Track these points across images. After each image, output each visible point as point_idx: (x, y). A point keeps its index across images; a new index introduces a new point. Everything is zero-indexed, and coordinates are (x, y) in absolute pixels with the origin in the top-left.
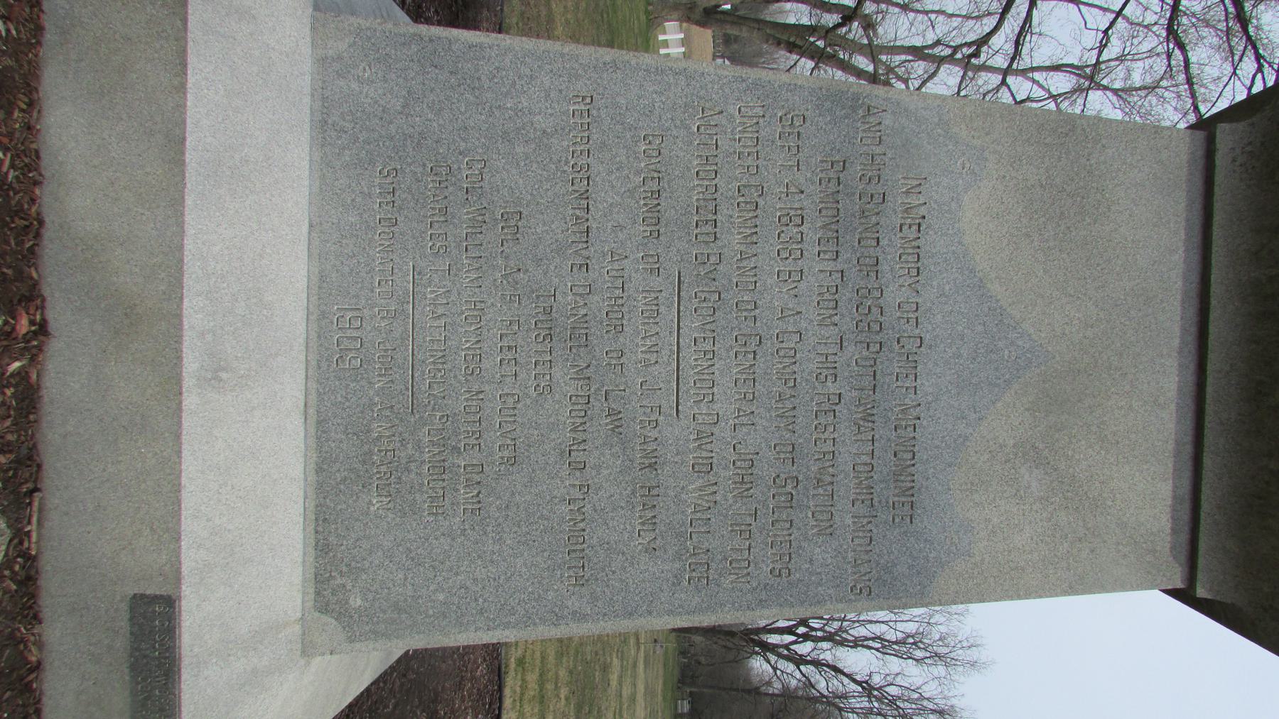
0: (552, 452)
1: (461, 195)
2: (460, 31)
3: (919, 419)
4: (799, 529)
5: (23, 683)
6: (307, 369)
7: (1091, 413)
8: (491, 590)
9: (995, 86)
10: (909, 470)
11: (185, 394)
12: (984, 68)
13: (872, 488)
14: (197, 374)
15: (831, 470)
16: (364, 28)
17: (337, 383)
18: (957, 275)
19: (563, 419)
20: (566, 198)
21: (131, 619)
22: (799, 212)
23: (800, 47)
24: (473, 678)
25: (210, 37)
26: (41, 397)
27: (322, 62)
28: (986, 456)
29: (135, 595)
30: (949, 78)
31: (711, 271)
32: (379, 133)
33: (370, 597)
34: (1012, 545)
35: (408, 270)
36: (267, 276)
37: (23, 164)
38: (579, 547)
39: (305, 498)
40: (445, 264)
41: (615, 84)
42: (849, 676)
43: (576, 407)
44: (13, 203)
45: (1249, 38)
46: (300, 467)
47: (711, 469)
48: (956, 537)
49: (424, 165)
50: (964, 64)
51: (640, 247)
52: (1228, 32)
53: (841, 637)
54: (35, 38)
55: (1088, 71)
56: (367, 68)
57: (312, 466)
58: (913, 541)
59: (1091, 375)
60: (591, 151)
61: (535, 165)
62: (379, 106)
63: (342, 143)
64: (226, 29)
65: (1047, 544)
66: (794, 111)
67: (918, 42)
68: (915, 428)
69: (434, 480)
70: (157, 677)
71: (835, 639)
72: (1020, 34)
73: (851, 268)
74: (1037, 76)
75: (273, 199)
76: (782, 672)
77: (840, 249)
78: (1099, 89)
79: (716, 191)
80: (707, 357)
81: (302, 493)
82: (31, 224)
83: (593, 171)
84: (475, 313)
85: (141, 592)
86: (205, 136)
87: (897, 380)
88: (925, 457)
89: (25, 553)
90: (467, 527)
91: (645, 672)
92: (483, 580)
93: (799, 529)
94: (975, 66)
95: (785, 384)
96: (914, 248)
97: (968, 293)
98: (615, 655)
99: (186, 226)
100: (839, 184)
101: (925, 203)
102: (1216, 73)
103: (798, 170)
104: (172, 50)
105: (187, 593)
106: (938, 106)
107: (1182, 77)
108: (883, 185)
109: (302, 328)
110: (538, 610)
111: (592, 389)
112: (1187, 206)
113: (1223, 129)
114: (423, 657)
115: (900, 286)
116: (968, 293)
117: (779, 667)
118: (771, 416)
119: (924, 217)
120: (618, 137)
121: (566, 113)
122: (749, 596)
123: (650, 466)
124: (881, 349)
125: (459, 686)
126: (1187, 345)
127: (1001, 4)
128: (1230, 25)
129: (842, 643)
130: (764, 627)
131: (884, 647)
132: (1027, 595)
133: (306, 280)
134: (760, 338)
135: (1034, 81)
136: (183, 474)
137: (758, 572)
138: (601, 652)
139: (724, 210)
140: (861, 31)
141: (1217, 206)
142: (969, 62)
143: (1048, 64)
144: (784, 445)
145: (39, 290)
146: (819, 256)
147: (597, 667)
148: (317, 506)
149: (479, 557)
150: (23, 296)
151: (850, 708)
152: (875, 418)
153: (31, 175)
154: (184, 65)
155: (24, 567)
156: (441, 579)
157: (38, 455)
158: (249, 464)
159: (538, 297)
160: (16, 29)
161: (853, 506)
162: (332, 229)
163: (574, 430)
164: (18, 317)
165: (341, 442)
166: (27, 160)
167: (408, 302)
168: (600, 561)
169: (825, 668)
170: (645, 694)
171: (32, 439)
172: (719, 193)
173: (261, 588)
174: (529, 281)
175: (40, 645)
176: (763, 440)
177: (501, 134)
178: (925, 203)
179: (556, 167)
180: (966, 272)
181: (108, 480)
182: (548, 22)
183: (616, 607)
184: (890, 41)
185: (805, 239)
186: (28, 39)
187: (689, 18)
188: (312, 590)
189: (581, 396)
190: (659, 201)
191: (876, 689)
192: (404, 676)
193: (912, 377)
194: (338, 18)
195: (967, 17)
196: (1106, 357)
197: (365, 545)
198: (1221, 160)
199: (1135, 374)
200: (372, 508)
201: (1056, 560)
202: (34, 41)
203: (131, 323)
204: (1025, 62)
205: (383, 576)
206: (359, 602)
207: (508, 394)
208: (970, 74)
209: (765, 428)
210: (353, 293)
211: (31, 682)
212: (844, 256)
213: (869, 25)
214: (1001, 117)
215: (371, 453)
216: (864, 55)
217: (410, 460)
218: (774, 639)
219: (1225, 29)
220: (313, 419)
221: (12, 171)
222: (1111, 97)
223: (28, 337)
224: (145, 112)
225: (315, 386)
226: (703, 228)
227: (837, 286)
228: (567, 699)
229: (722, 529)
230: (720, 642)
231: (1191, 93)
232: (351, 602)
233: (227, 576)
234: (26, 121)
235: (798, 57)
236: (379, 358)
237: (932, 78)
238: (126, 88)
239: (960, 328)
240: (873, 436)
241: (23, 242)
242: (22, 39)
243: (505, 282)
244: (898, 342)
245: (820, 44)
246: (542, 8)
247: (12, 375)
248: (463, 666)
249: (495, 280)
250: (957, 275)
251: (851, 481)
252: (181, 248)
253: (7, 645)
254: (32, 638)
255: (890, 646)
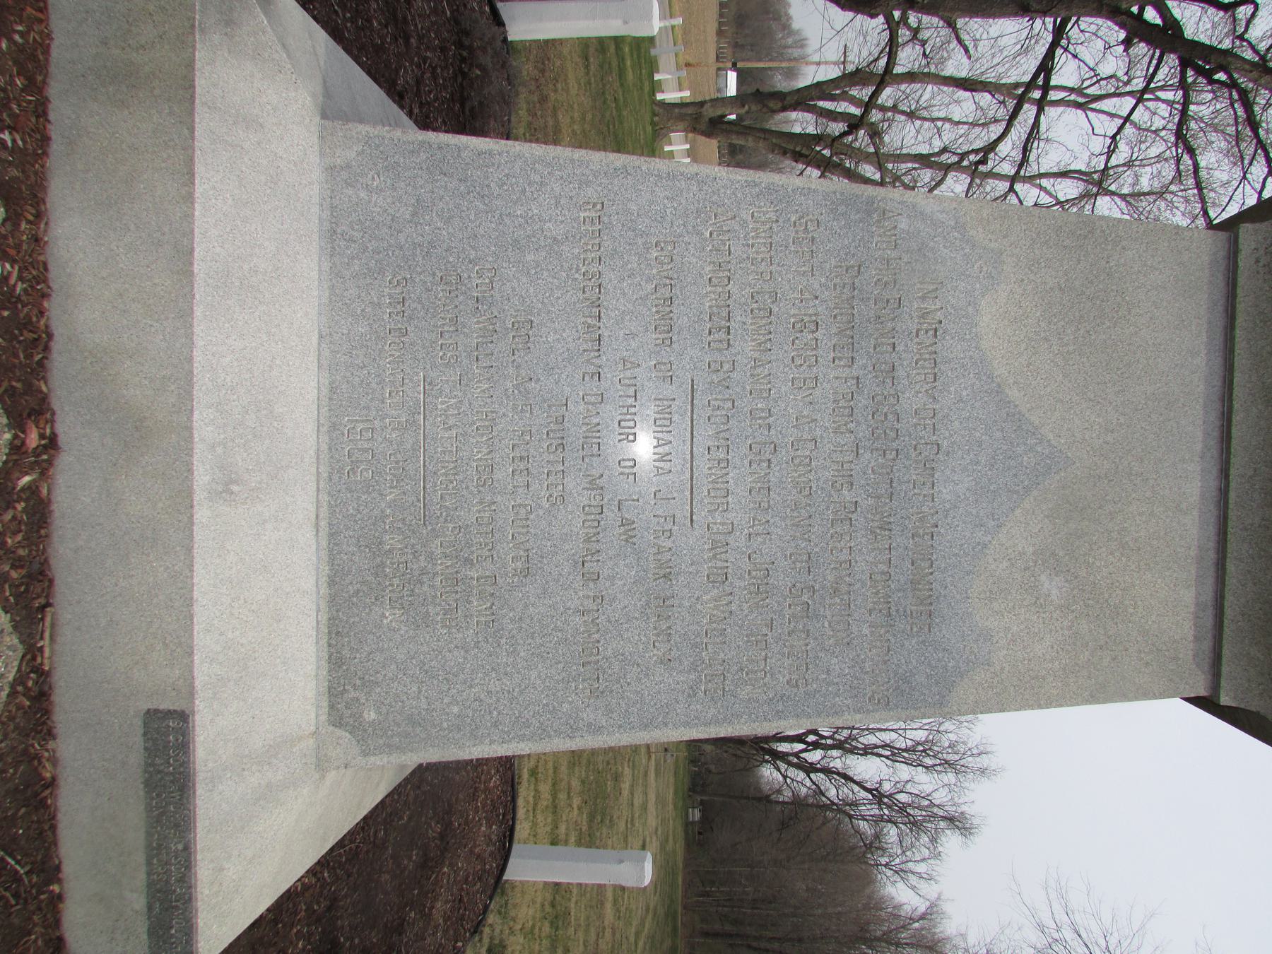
0: (566, 563)
1: (472, 303)
2: (469, 138)
3: (937, 526)
4: (816, 639)
5: (38, 798)
6: (318, 481)
7: (1112, 519)
9: (1002, 193)
10: (927, 579)
11: (196, 508)
12: (991, 175)
13: (890, 597)
14: (208, 487)
15: (847, 579)
16: (372, 135)
17: (348, 495)
18: (974, 380)
20: (577, 306)
21: (145, 734)
22: (814, 318)
23: (807, 156)
24: (487, 789)
25: (218, 146)
26: (52, 511)
27: (331, 170)
28: (1005, 564)
29: (149, 710)
30: (956, 184)
31: (724, 379)
33: (384, 710)
34: (1032, 654)
35: (419, 381)
36: (277, 387)
37: (30, 277)
38: (593, 658)
39: (318, 612)
40: (456, 373)
41: (626, 190)
42: (858, 784)
43: (589, 517)
44: (22, 315)
45: (1259, 141)
46: (312, 580)
47: (726, 578)
48: (975, 646)
49: (434, 274)
50: (970, 172)
51: (653, 355)
52: (1238, 138)
53: (851, 745)
54: (41, 149)
55: (1096, 176)
56: (376, 176)
57: (325, 579)
58: (932, 651)
59: (1112, 481)
60: (603, 259)
61: (546, 274)
62: (388, 215)
63: (351, 252)
64: (234, 138)
66: (808, 215)
67: (924, 150)
68: (932, 536)
69: (447, 592)
70: (172, 792)
71: (846, 746)
72: (1028, 140)
73: (867, 375)
74: (1045, 182)
75: (282, 310)
76: (792, 780)
77: (855, 355)
78: (1106, 195)
79: (729, 297)
80: (722, 465)
81: (314, 607)
82: (40, 337)
83: (605, 280)
84: (487, 423)
85: (155, 707)
86: (213, 247)
87: (914, 487)
88: (943, 565)
89: (38, 669)
90: (480, 639)
91: (656, 781)
92: (498, 692)
93: (816, 639)
94: (982, 173)
95: (801, 493)
96: (930, 353)
97: (986, 399)
98: (626, 765)
99: (195, 337)
100: (854, 289)
101: (942, 308)
102: (1225, 177)
103: (813, 275)
104: (179, 159)
105: (201, 708)
106: (955, 208)
107: (1191, 182)
108: (899, 290)
109: (312, 440)
110: (552, 723)
111: (605, 500)
112: (1208, 308)
113: (1246, 229)
114: (437, 769)
115: (917, 392)
116: (986, 399)
117: (789, 775)
118: (786, 525)
119: (941, 322)
121: (576, 219)
122: (766, 708)
123: (665, 576)
124: (897, 456)
125: (474, 797)
126: (1209, 450)
127: (1008, 111)
128: (1240, 129)
129: (853, 751)
130: (774, 736)
131: (894, 754)
132: (1049, 704)
133: (316, 391)
134: (775, 447)
135: (1041, 188)
136: (195, 588)
137: (775, 683)
138: (613, 762)
139: (738, 317)
140: (867, 138)
141: (1240, 307)
142: (976, 168)
143: (1055, 170)
144: (800, 555)
145: (49, 404)
146: (834, 362)
147: (609, 776)
148: (330, 619)
149: (493, 669)
150: (34, 410)
151: (861, 815)
152: (893, 526)
153: (39, 287)
154: (191, 174)
155: (37, 683)
156: (454, 691)
157: (50, 570)
158: (261, 578)
159: (549, 407)
160: (23, 140)
161: (870, 615)
162: (342, 339)
163: (588, 540)
164: (28, 431)
165: (353, 554)
166: (34, 273)
167: (419, 413)
169: (835, 776)
170: (656, 804)
171: (43, 554)
173: (275, 702)
175: (54, 761)
176: (778, 549)
178: (942, 308)
179: (568, 275)
181: (120, 595)
182: (555, 134)
183: (632, 719)
184: (897, 149)
185: (819, 345)
186: (35, 150)
187: (695, 129)
188: (325, 704)
189: (594, 506)
190: (671, 308)
191: (886, 797)
192: (419, 788)
193: (929, 485)
194: (346, 126)
195: (974, 125)
196: (1126, 462)
197: (379, 657)
198: (1244, 261)
199: (1156, 480)
200: (385, 621)
202: (40, 152)
203: (141, 436)
204: (1032, 169)
205: (396, 690)
206: (373, 715)
207: (520, 505)
208: (978, 181)
209: (780, 537)
210: (363, 404)
211: (46, 798)
212: (861, 362)
213: (875, 134)
215: (382, 565)
216: (871, 163)
217: (423, 572)
218: (784, 747)
219: (1234, 133)
220: (324, 533)
221: (20, 283)
222: (1119, 203)
223: (38, 451)
224: (153, 223)
225: (326, 499)
226: (716, 335)
227: (852, 393)
228: (579, 809)
230: (731, 751)
231: (1201, 199)
232: (365, 715)
234: (34, 232)
235: (804, 166)
236: (390, 469)
237: (939, 186)
238: (134, 198)
239: (978, 434)
240: (891, 544)
241: (32, 355)
242: (29, 149)
243: (516, 392)
244: (915, 449)
245: (827, 152)
246: (549, 119)
247: (23, 489)
248: (477, 777)
249: (506, 390)
250: (974, 380)
251: (867, 590)
252: (190, 360)
253: (21, 761)
254: (46, 754)
255: (899, 753)
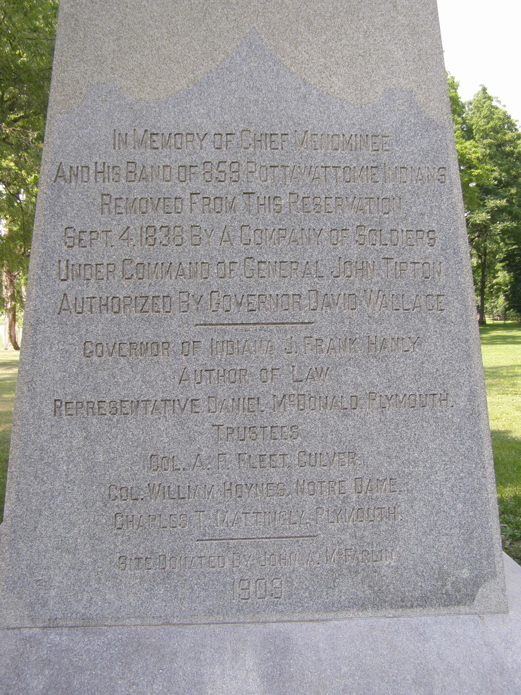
8: (453, 467)
18: (192, 104)
19: (318, 415)
28: (334, 79)
32: (91, 571)
39: (385, 616)
41: (45, 382)
51: (178, 357)
58: (403, 135)
61: (114, 445)
65: (399, 32)
73: (189, 187)
87: (277, 149)
92: (446, 473)
100: (121, 198)
110: (469, 429)
111: (294, 393)
120: (88, 378)
122: (452, 262)
137: (432, 256)
139: (145, 290)
156: (446, 507)
165: (341, 591)
168: (429, 382)
172: (132, 295)
174: (208, 447)
176: (329, 254)
177: (89, 473)
179: (114, 427)
180: (190, 96)
185: (166, 225)
188: (457, 608)
197: (421, 568)
201: (411, 25)
210: (222, 588)
214: (64, 73)
215: (349, 568)
227: (204, 198)
229: (400, 285)
232: (465, 576)
233: (452, 672)
243: (209, 466)
250: (192, 104)
